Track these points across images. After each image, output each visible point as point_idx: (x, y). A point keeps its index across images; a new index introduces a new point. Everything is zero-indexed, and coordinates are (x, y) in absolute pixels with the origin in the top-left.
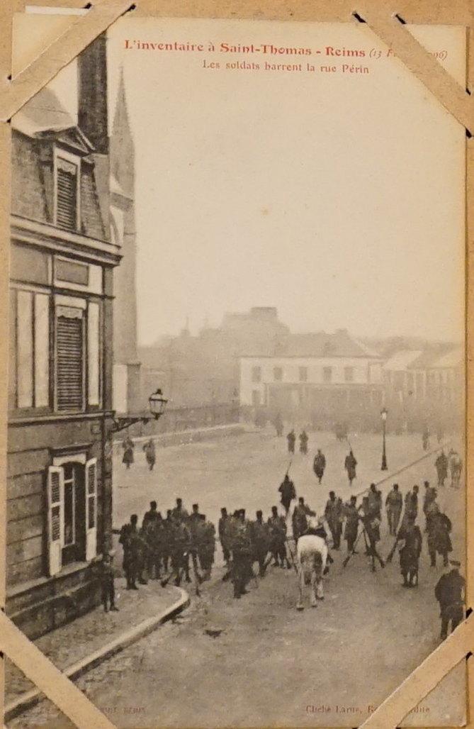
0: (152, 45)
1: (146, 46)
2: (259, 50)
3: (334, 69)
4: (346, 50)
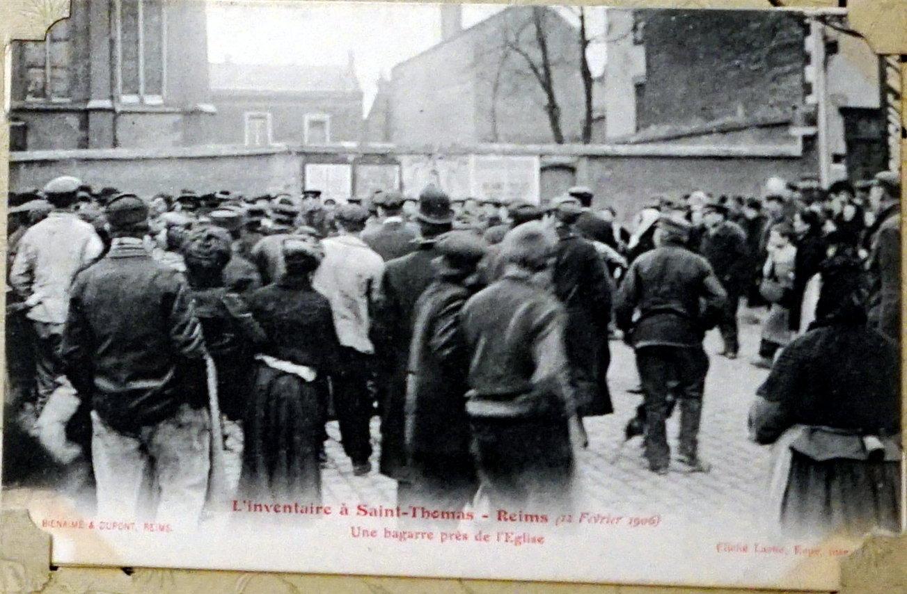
3: (373, 534)
4: (524, 513)
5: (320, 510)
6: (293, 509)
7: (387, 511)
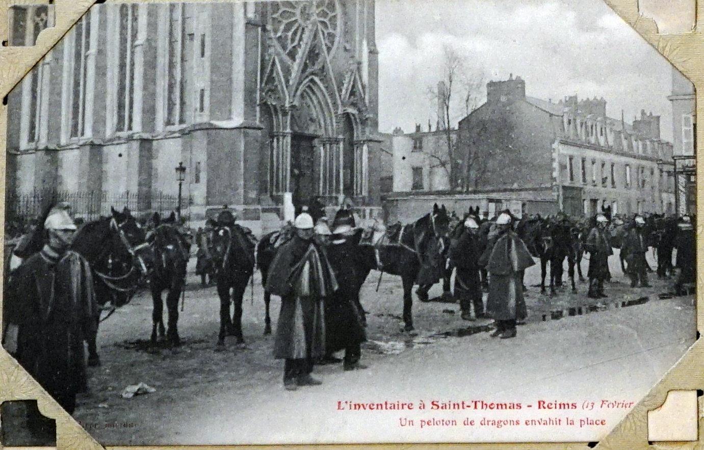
0: (363, 405)
2: (469, 406)
4: (558, 403)
5: (405, 406)
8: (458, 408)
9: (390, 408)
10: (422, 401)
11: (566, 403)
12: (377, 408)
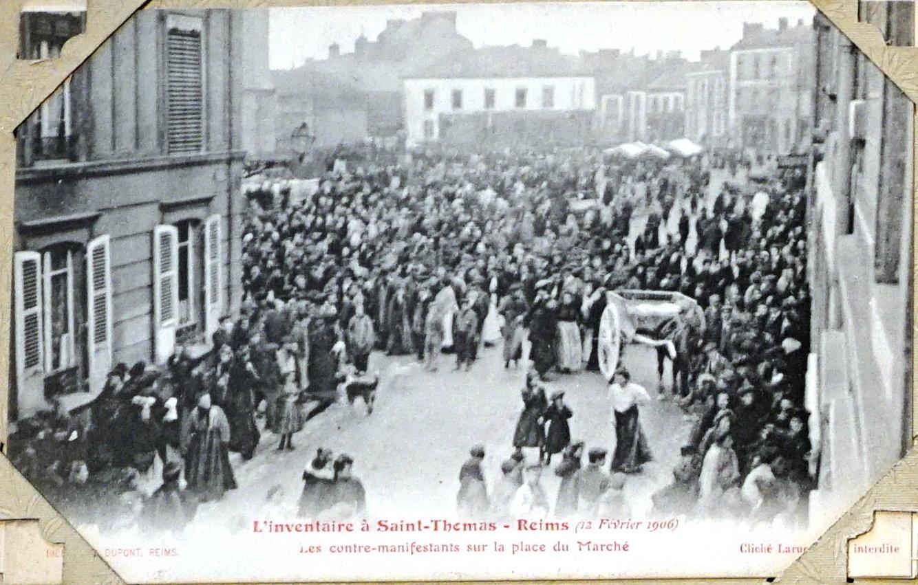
0: (287, 526)
1: (279, 528)
2: (426, 527)
4: (405, 524)
5: (342, 527)
6: (315, 529)
7: (408, 525)
8: (282, 531)
9: (323, 530)
10: (364, 521)
11: (554, 522)
12: (306, 530)
